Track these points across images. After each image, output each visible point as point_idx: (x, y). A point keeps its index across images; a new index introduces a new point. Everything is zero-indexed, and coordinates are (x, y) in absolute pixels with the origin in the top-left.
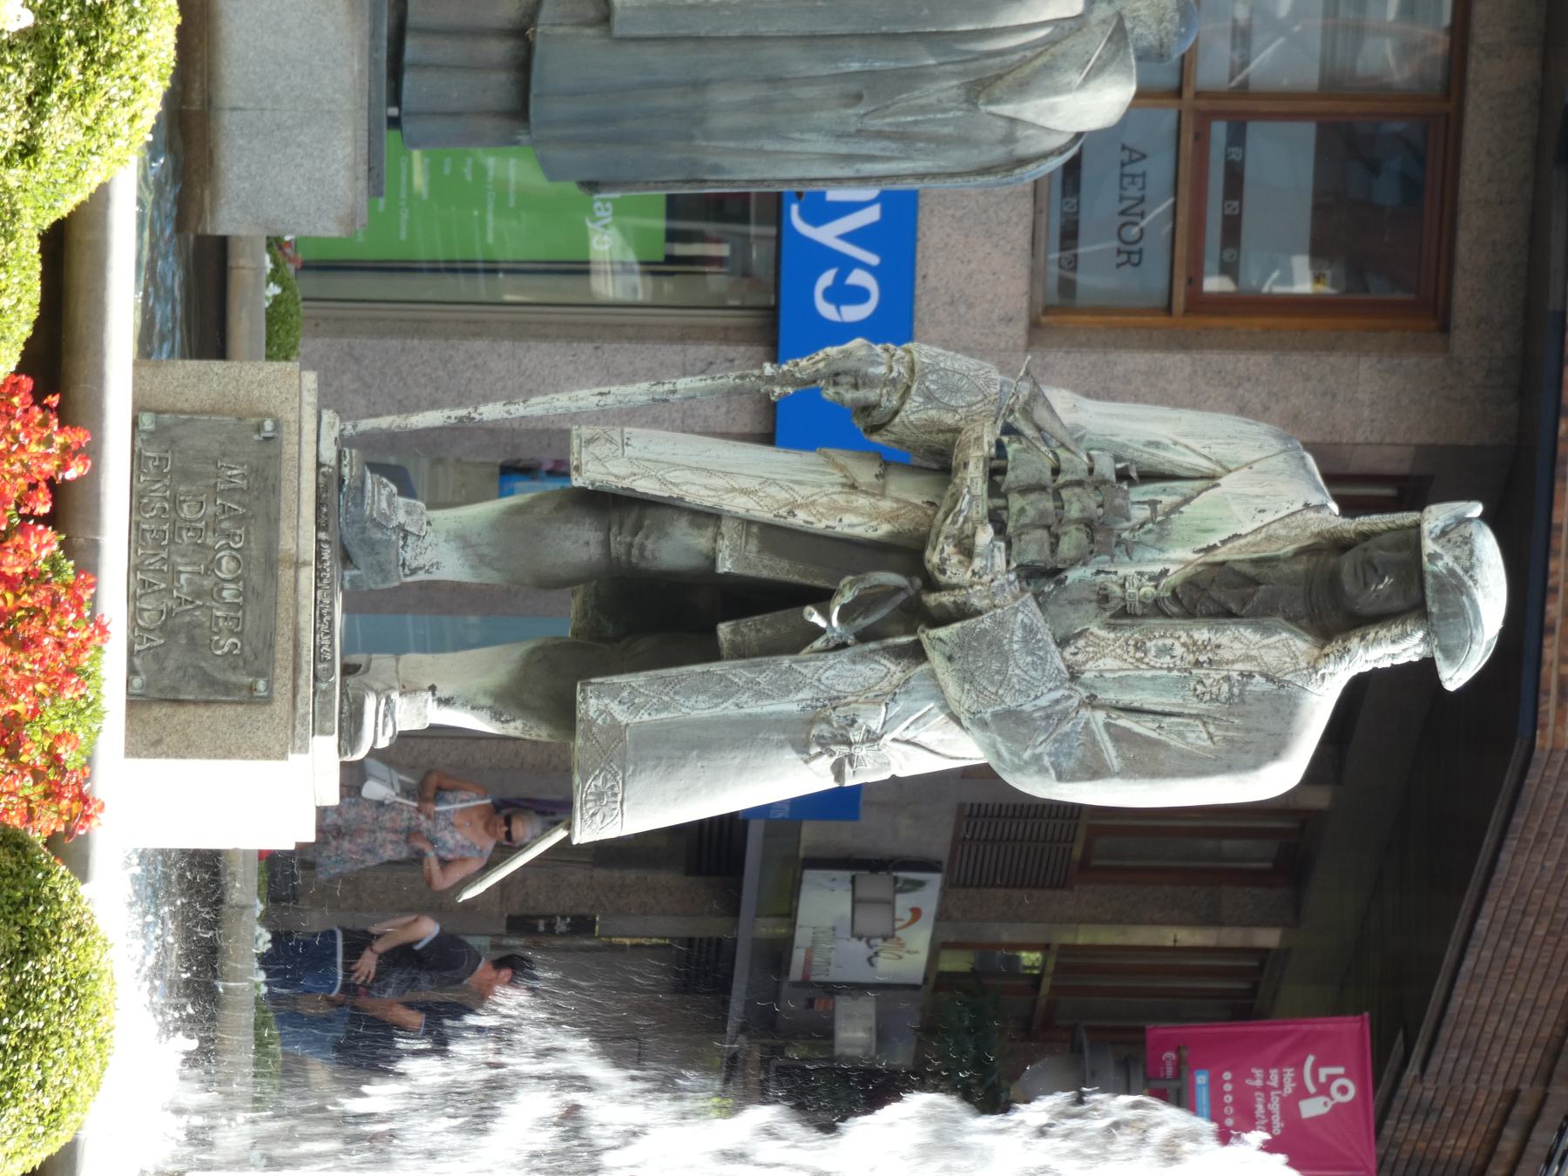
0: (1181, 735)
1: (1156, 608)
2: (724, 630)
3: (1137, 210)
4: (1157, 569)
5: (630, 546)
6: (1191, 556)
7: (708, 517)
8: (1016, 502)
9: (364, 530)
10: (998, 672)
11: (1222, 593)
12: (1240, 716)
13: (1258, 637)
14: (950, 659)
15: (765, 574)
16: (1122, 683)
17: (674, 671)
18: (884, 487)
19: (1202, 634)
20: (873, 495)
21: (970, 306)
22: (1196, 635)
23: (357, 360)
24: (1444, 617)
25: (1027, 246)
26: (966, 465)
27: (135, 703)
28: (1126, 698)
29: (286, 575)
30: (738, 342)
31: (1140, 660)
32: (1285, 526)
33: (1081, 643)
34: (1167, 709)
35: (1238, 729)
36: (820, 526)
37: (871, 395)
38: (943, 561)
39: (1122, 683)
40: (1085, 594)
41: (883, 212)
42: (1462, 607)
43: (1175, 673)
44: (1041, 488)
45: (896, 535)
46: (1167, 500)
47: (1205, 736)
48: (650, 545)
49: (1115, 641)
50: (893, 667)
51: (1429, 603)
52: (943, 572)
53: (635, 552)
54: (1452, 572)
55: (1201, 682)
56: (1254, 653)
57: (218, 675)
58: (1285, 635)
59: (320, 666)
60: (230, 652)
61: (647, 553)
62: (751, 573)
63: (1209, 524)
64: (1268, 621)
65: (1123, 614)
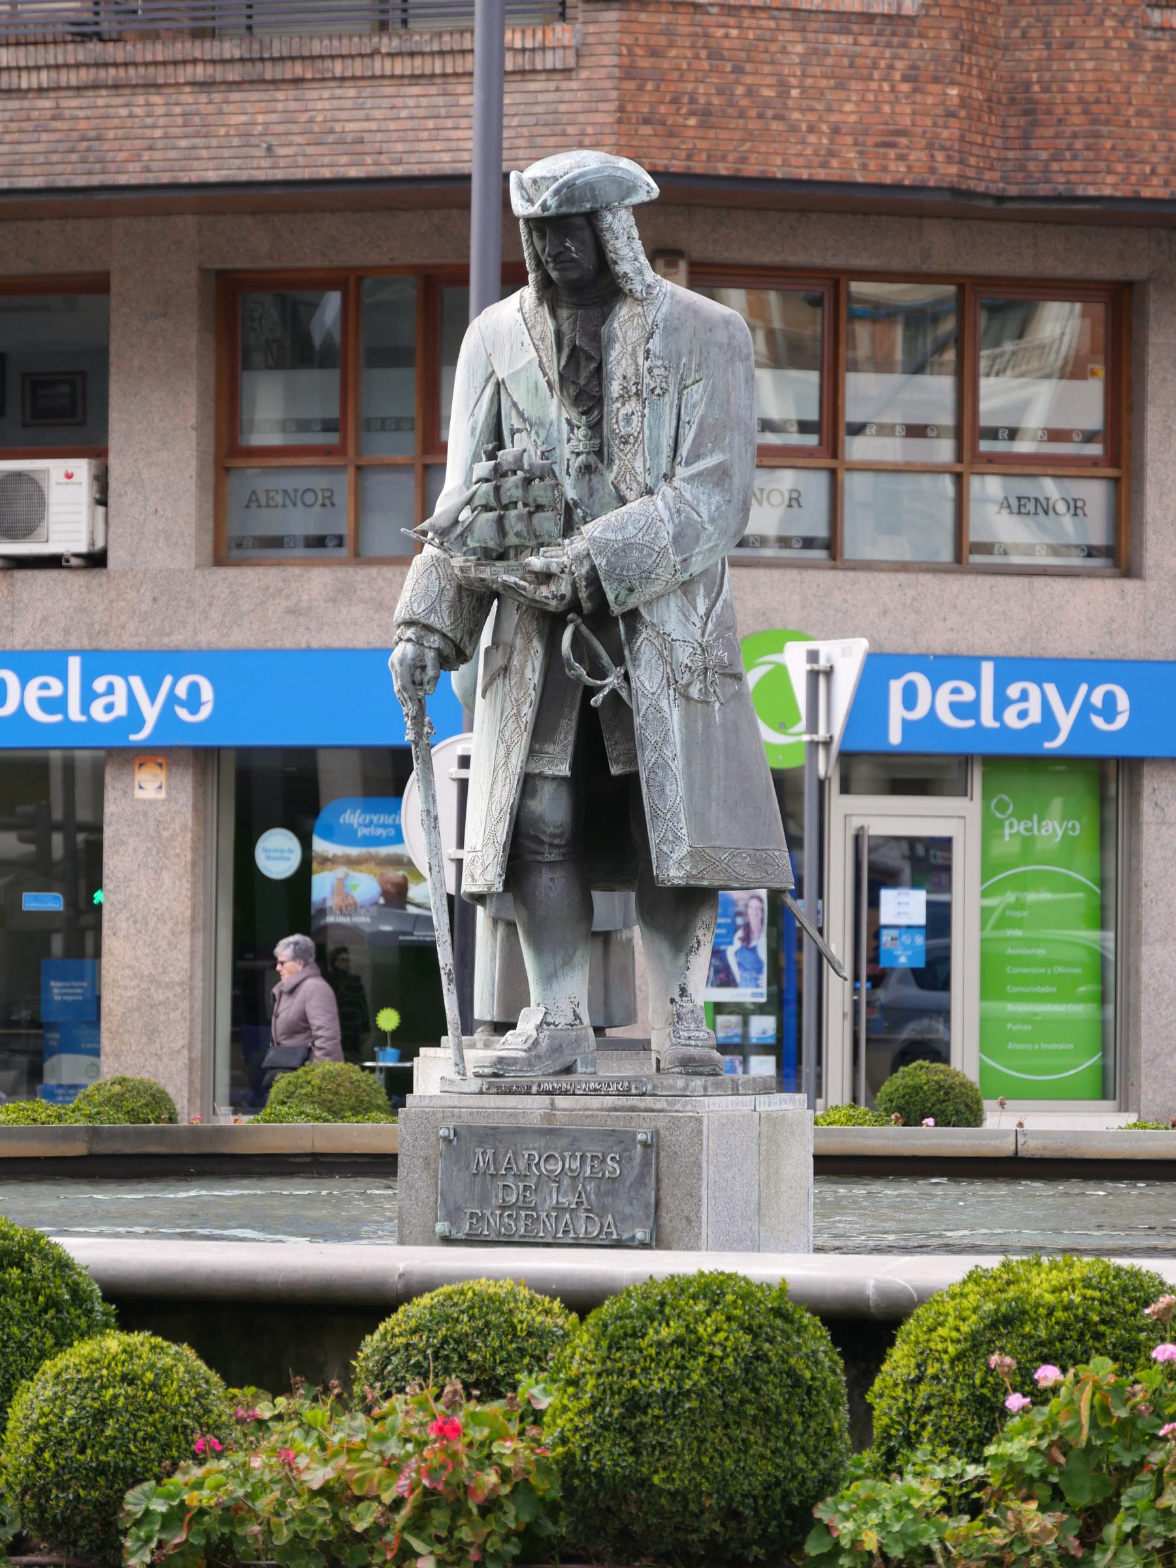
0: (694, 406)
1: (595, 428)
2: (615, 770)
3: (1044, 503)
4: (565, 427)
5: (551, 845)
6: (556, 400)
7: (528, 784)
8: (512, 540)
9: (538, 1057)
10: (641, 552)
11: (583, 377)
12: (680, 359)
13: (617, 346)
14: (631, 590)
15: (571, 738)
16: (656, 453)
17: (647, 810)
18: (505, 644)
19: (615, 388)
20: (512, 653)
21: (1113, 620)
22: (616, 395)
23: (1157, 1056)
24: (594, 198)
25: (1069, 580)
26: (483, 580)
27: (657, 1241)
28: (666, 451)
29: (559, 1122)
30: (1141, 785)
31: (636, 439)
32: (534, 326)
33: (623, 486)
34: (674, 417)
35: (690, 361)
36: (533, 695)
37: (430, 655)
38: (555, 597)
39: (656, 453)
40: (585, 484)
41: (1049, 681)
42: (586, 184)
43: (646, 411)
44: (500, 520)
45: (541, 636)
46: (517, 423)
47: (695, 387)
48: (550, 830)
49: (620, 459)
50: (644, 635)
51: (583, 210)
52: (563, 597)
53: (557, 841)
54: (557, 192)
55: (653, 391)
56: (630, 348)
57: (636, 1172)
58: (616, 325)
59: (633, 1091)
60: (618, 1162)
61: (558, 831)
62: (570, 749)
63: (532, 386)
64: (604, 339)
65: (599, 454)
